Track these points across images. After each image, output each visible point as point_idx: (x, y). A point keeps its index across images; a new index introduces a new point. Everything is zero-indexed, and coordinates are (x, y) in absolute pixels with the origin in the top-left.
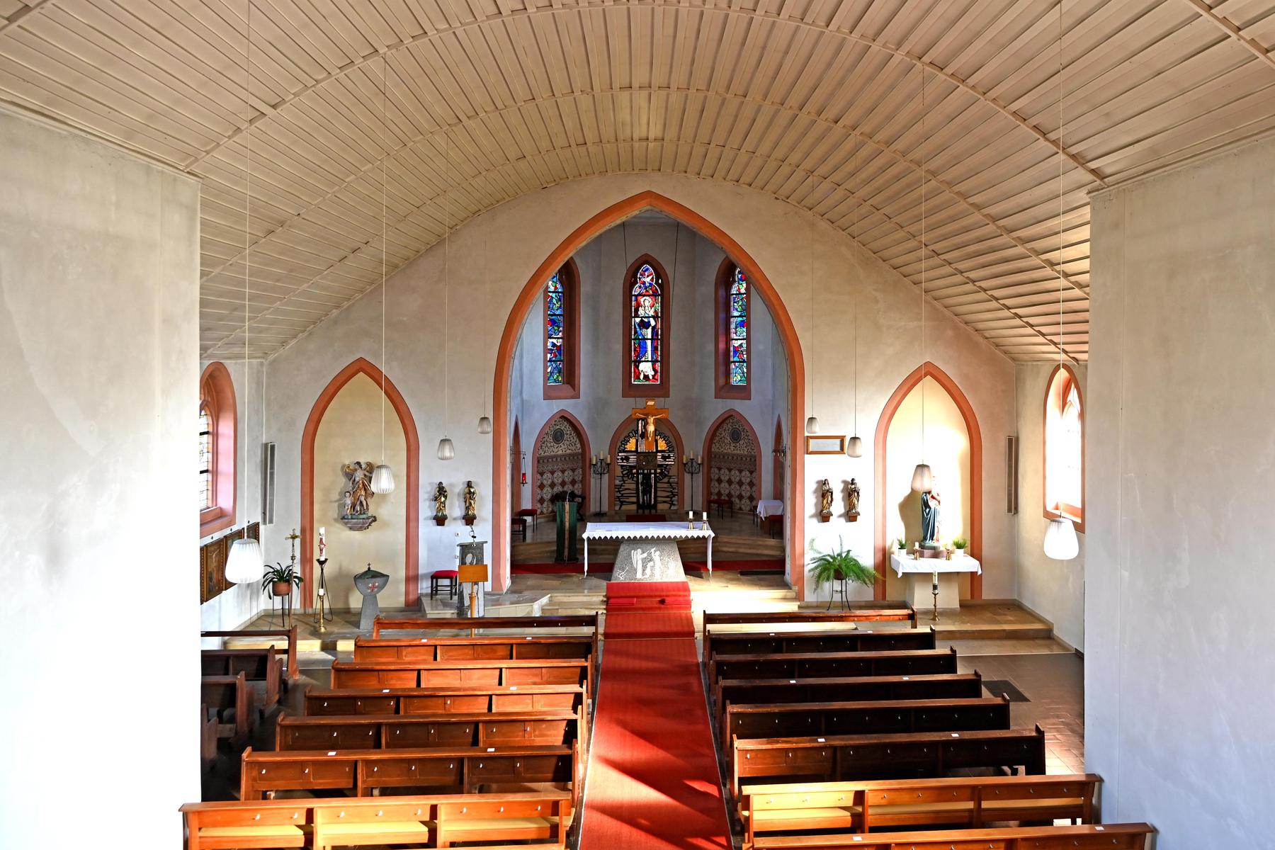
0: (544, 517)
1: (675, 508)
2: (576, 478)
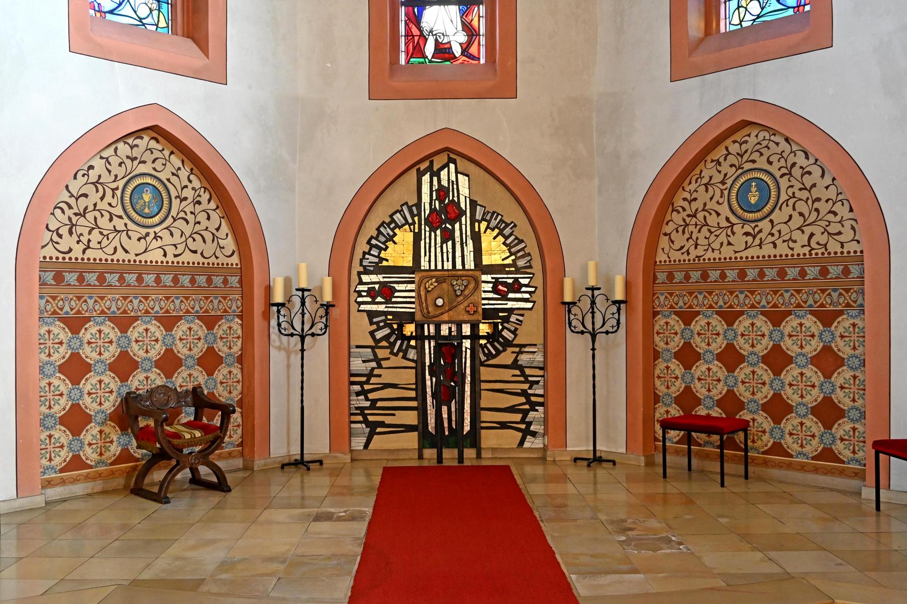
0: (87, 478)
1: (538, 443)
2: (221, 348)
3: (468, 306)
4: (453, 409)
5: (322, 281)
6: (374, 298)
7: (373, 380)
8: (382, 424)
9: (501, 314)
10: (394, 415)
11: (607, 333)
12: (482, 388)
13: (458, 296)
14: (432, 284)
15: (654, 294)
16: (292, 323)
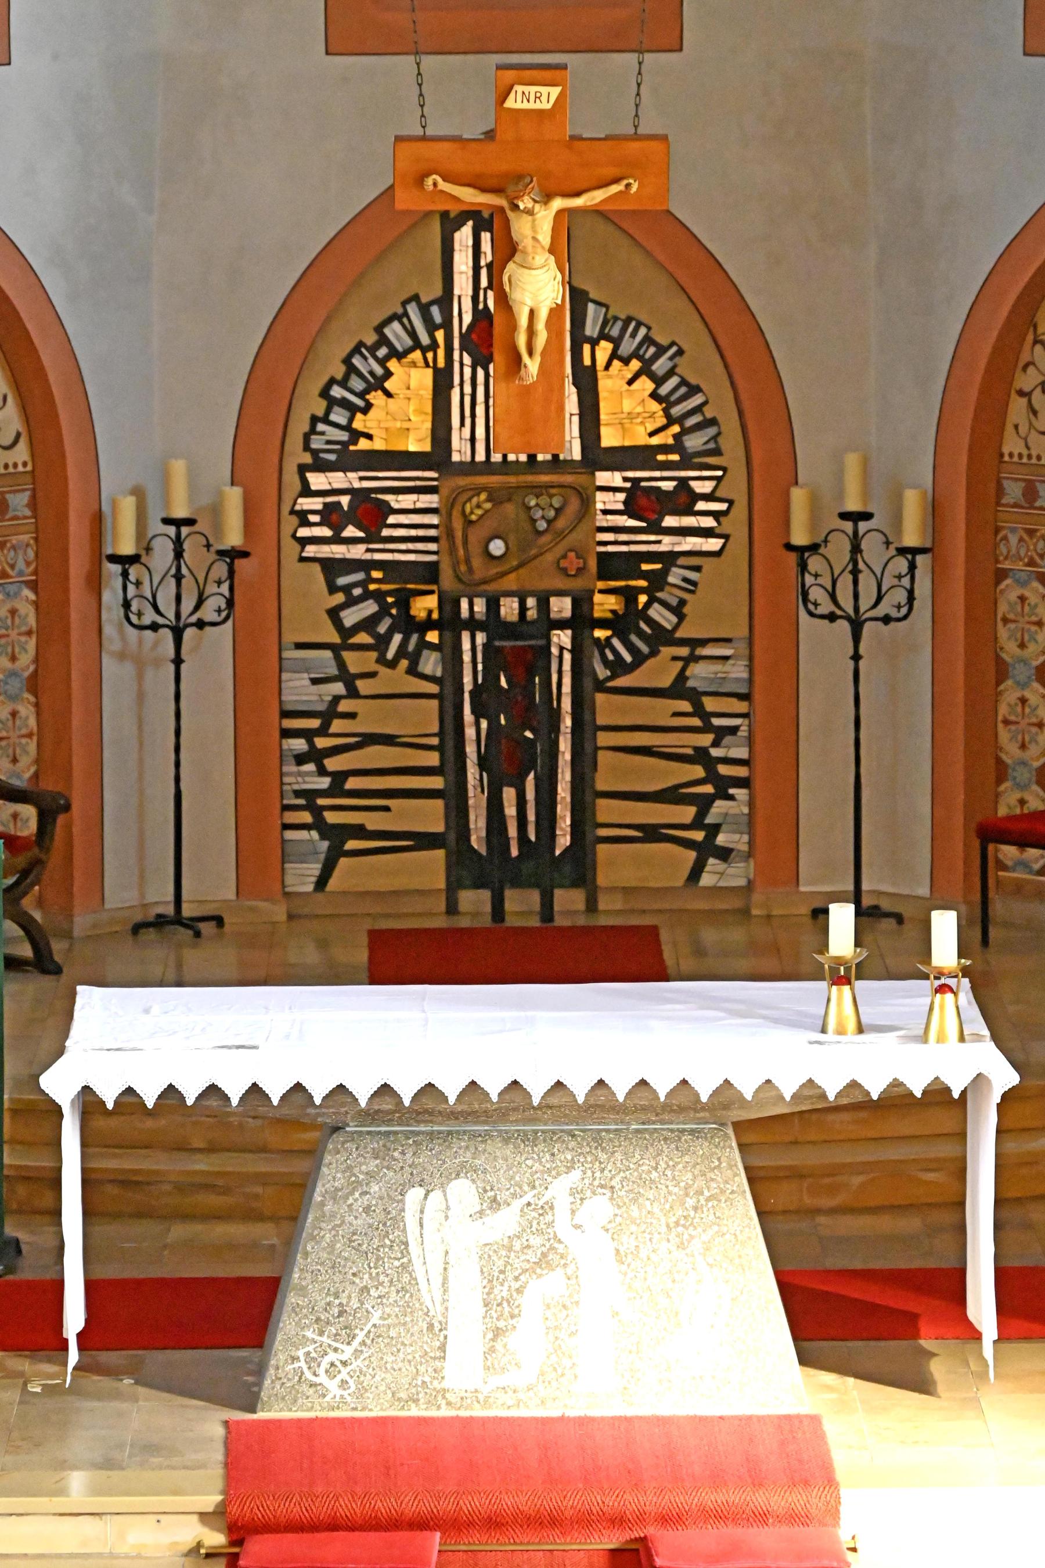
3: (564, 556)
4: (530, 795)
5: (220, 494)
6: (337, 529)
7: (337, 725)
8: (359, 831)
9: (645, 567)
10: (387, 809)
11: (886, 620)
12: (600, 744)
13: (540, 533)
14: (478, 506)
15: (997, 530)
16: (154, 596)
